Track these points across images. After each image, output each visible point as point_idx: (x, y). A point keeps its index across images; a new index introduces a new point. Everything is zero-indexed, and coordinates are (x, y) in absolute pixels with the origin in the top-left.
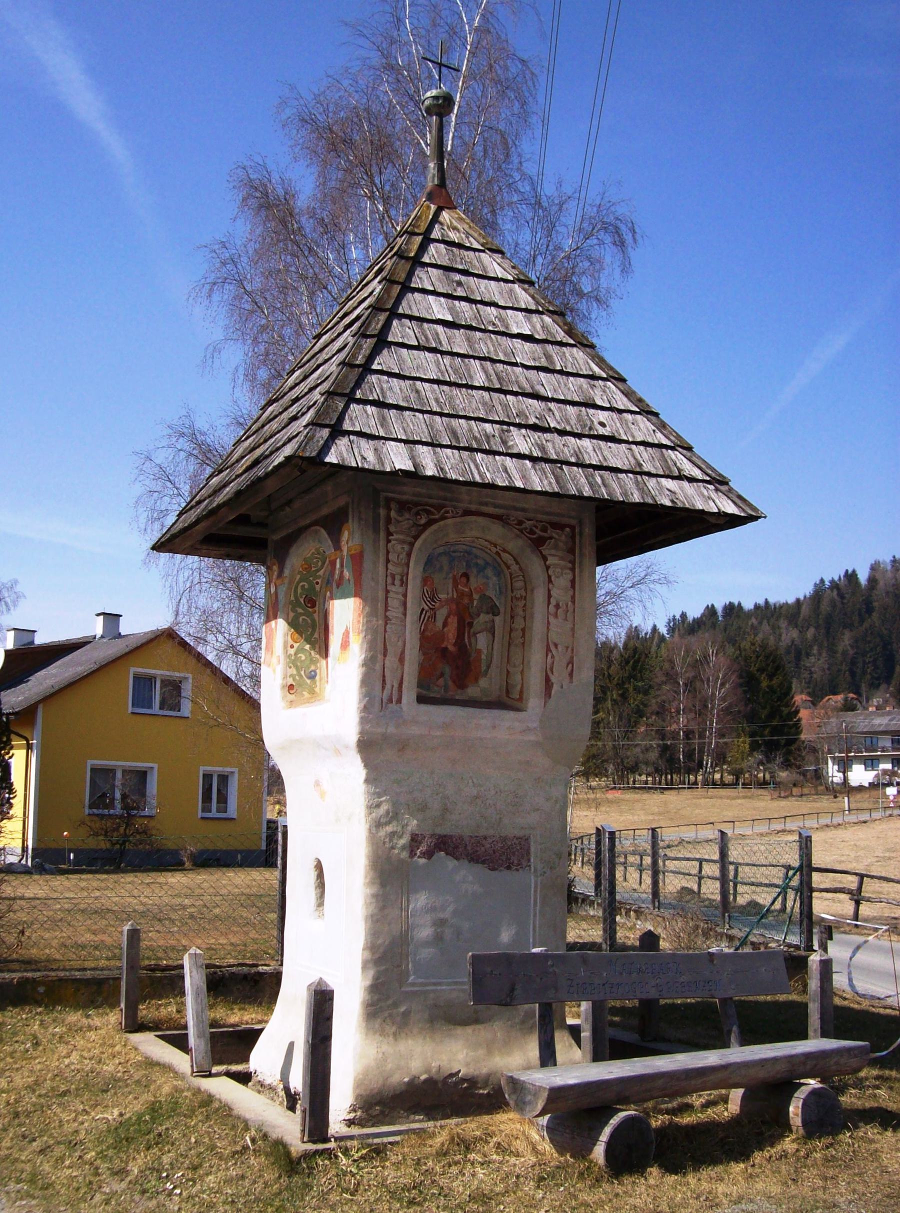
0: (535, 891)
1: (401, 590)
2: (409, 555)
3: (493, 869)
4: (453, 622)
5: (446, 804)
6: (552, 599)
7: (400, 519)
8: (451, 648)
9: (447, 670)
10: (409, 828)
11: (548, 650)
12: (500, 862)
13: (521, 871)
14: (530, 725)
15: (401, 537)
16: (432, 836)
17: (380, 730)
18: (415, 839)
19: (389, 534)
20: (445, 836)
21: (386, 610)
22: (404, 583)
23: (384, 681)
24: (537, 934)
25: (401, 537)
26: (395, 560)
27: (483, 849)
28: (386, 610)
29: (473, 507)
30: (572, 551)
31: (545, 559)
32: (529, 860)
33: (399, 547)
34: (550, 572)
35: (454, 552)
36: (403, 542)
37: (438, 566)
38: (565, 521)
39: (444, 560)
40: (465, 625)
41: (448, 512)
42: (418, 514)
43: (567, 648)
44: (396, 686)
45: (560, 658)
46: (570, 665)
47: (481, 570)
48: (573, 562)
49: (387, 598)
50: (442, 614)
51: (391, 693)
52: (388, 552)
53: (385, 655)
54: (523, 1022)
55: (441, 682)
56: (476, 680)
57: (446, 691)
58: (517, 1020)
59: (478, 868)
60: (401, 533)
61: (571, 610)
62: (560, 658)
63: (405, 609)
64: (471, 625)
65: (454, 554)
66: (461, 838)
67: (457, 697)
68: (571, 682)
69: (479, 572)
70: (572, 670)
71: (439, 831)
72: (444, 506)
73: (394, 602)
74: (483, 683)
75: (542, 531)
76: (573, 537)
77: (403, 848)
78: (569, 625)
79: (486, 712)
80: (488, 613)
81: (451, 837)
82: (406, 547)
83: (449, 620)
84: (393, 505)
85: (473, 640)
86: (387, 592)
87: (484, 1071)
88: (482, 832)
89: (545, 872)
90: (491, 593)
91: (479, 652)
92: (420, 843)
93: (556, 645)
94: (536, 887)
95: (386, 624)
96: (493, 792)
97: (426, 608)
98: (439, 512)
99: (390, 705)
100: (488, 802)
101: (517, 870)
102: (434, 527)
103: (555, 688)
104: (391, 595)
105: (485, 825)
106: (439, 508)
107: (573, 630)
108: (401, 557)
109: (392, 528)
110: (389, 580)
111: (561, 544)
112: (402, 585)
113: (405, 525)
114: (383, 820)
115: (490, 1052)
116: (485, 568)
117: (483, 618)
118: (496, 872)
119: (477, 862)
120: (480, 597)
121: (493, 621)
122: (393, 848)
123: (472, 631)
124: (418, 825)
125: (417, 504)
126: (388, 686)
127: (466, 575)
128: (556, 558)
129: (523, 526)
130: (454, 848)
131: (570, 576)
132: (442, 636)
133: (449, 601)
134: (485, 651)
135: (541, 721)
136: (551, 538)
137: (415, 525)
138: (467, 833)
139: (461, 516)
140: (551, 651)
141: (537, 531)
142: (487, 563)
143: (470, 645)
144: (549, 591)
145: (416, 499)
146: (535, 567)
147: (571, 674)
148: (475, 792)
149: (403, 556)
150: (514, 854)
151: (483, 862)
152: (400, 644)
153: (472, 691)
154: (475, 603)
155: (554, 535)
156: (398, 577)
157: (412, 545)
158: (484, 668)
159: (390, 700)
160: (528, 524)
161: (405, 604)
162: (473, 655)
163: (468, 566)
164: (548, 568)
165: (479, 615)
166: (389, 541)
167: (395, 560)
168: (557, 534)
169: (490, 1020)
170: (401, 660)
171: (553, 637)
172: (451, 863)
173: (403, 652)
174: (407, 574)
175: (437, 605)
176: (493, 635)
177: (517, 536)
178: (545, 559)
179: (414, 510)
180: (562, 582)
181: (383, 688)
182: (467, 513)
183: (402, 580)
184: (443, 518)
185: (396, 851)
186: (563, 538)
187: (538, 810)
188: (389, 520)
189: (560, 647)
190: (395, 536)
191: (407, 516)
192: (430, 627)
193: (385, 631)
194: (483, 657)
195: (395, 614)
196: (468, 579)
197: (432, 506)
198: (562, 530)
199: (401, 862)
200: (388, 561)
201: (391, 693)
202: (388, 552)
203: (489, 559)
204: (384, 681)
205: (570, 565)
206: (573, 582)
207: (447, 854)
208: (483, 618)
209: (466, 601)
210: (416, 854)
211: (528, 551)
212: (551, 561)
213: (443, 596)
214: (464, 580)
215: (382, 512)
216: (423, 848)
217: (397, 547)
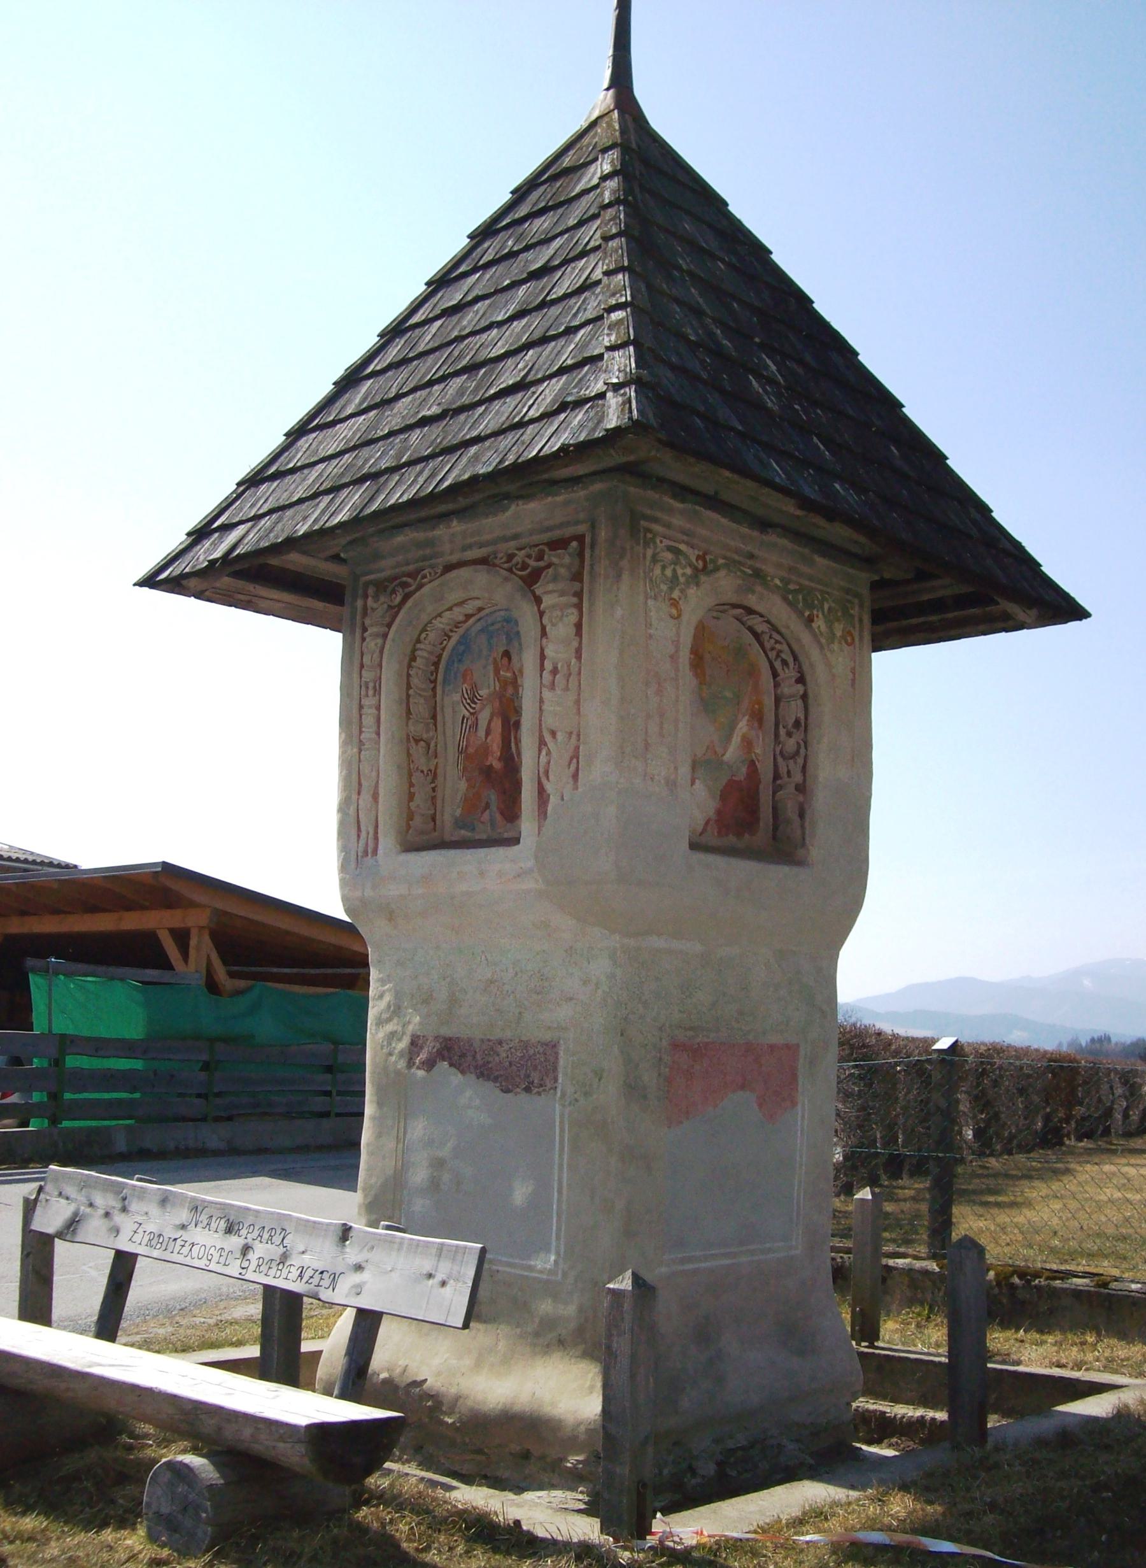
0: (562, 1130)
3: (507, 1091)
4: (497, 724)
6: (546, 662)
8: (497, 765)
10: (411, 1027)
12: (518, 1080)
16: (436, 1038)
17: (358, 894)
18: (416, 1043)
19: (365, 630)
20: (450, 1039)
21: (361, 732)
22: (377, 691)
24: (564, 1198)
27: (497, 1058)
29: (454, 558)
30: (577, 577)
31: (538, 600)
32: (556, 1080)
36: (377, 635)
38: (569, 531)
41: (424, 577)
43: (571, 733)
44: (371, 835)
46: (575, 761)
48: (579, 595)
50: (484, 717)
53: (359, 794)
54: (537, 1334)
58: (529, 1329)
59: (489, 1089)
61: (574, 670)
62: (559, 749)
63: (379, 727)
65: (491, 628)
66: (470, 1041)
68: (576, 788)
70: (577, 769)
71: (446, 1031)
76: (581, 555)
77: (401, 1054)
78: (572, 696)
82: (380, 641)
83: (493, 724)
86: (361, 707)
87: (453, 1390)
88: (497, 1034)
89: (576, 1100)
92: (422, 1048)
94: (562, 1122)
95: (360, 751)
98: (415, 579)
100: (507, 987)
101: (539, 1093)
103: (553, 800)
104: (364, 711)
109: (367, 622)
111: (562, 571)
112: (374, 695)
113: (380, 612)
114: (385, 1016)
115: (478, 1365)
118: (510, 1095)
119: (488, 1079)
122: (390, 1054)
124: (420, 1023)
126: (363, 834)
128: (556, 595)
129: (514, 561)
131: (573, 618)
132: (485, 750)
135: (536, 857)
136: (549, 566)
140: (546, 744)
144: (542, 650)
146: (526, 614)
147: (575, 776)
150: (535, 1068)
151: (496, 1079)
152: (374, 774)
155: (555, 560)
156: (371, 685)
157: (385, 636)
159: (366, 853)
164: (541, 614)
169: (495, 1321)
170: (375, 797)
171: (549, 721)
172: (456, 1078)
175: (478, 707)
177: (506, 579)
180: (561, 629)
181: (359, 836)
182: (449, 568)
183: (375, 687)
184: (420, 586)
185: (393, 1058)
186: (567, 560)
187: (571, 999)
196: (510, 659)
197: (409, 575)
199: (398, 1073)
200: (362, 666)
201: (367, 844)
205: (575, 600)
206: (579, 626)
207: (451, 1065)
210: (414, 1064)
212: (547, 601)
216: (423, 1056)
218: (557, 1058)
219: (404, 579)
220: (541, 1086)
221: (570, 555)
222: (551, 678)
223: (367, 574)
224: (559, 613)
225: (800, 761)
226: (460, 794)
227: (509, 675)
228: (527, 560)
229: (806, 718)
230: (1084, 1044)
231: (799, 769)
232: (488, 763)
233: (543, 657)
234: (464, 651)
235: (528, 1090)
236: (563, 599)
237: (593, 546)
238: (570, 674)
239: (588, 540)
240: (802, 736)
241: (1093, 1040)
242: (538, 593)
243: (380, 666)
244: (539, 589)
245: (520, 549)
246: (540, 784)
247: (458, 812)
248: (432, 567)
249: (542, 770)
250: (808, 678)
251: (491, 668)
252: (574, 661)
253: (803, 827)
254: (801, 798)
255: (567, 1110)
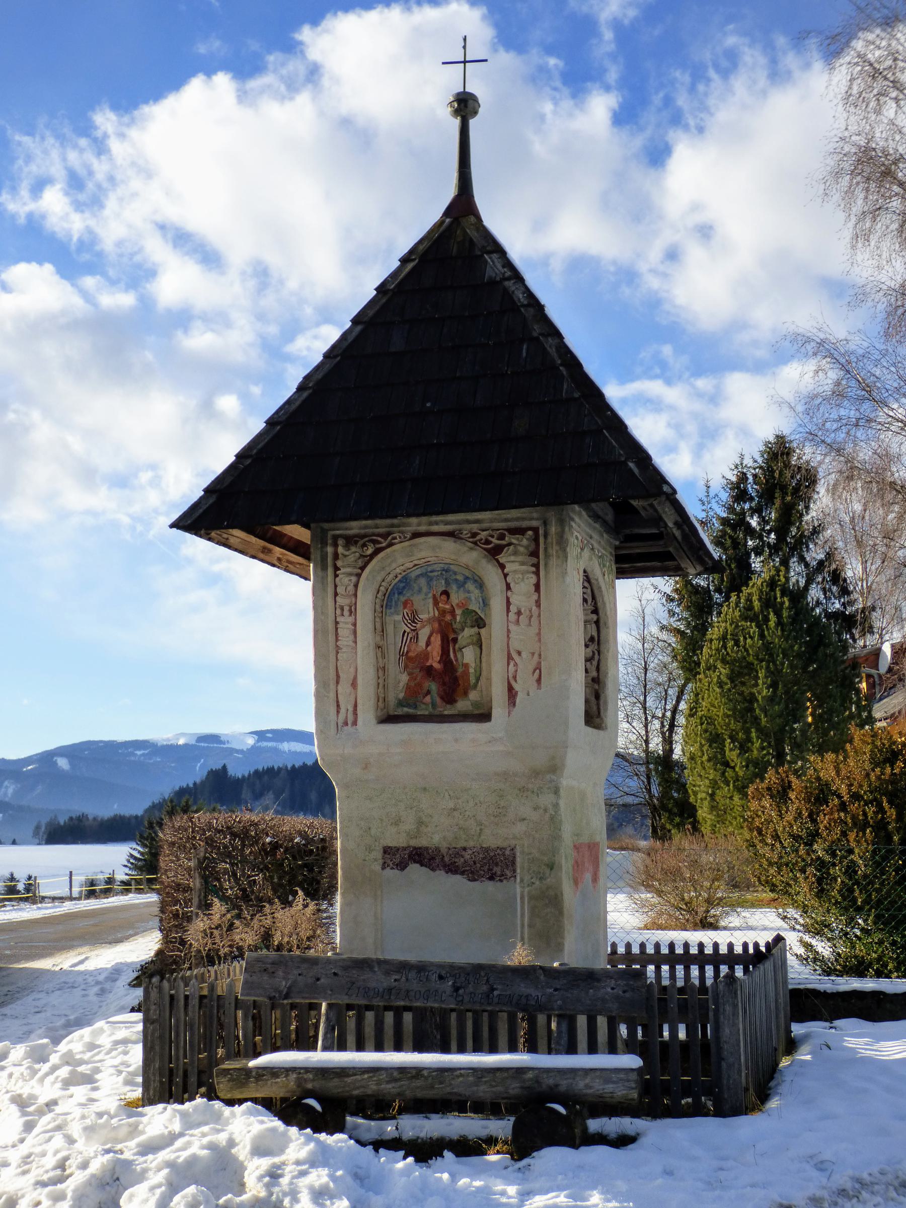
1: (351, 619)
2: (356, 586)
4: (437, 641)
5: (420, 818)
7: (347, 553)
8: (437, 666)
9: (434, 687)
11: (510, 658)
12: (482, 873)
13: (505, 882)
14: (494, 736)
15: (349, 570)
19: (336, 569)
20: (420, 848)
21: (337, 640)
22: (353, 611)
23: (338, 706)
25: (349, 570)
26: (343, 593)
27: (462, 860)
28: (337, 640)
30: (535, 554)
31: (502, 567)
32: (514, 871)
33: (346, 580)
34: (509, 579)
35: (431, 572)
37: (416, 588)
38: (525, 524)
39: (423, 581)
40: (448, 640)
41: (395, 538)
42: (364, 545)
43: (533, 654)
44: (351, 709)
45: (525, 665)
47: (461, 585)
48: (537, 566)
49: (337, 629)
50: (424, 634)
51: (347, 717)
52: (336, 586)
55: (428, 699)
56: (466, 694)
57: (434, 705)
60: (349, 566)
62: (525, 665)
63: (355, 637)
64: (455, 640)
66: (438, 849)
67: (446, 713)
69: (459, 588)
71: (414, 843)
72: (389, 534)
73: (345, 631)
74: (473, 695)
75: (498, 539)
76: (536, 540)
78: (534, 630)
79: (445, 726)
80: (472, 627)
81: (427, 848)
82: (354, 579)
83: (432, 638)
84: (341, 542)
85: (459, 655)
86: (337, 623)
88: (461, 844)
90: (473, 606)
91: (466, 666)
93: (519, 653)
94: (522, 898)
96: (471, 804)
97: (408, 630)
99: (346, 728)
101: (501, 881)
102: (381, 555)
105: (464, 836)
106: (385, 536)
107: (539, 634)
108: (349, 588)
109: (339, 563)
110: (338, 612)
111: (521, 549)
112: (350, 615)
113: (352, 558)
116: (465, 583)
117: (468, 632)
120: (463, 611)
121: (479, 634)
123: (457, 646)
125: (363, 536)
126: (343, 710)
127: (446, 593)
129: (478, 538)
130: (430, 860)
131: (533, 580)
132: (426, 655)
133: (429, 621)
134: (473, 665)
136: (510, 544)
137: (362, 556)
138: (444, 846)
139: (411, 539)
140: (513, 659)
141: (494, 540)
142: (467, 578)
143: (457, 660)
145: (363, 531)
147: (539, 681)
148: (451, 805)
149: (351, 588)
150: (497, 865)
151: (462, 873)
152: (352, 670)
153: (462, 705)
154: (458, 618)
155: (514, 541)
157: (359, 576)
158: (472, 680)
160: (483, 535)
161: (355, 633)
162: (460, 670)
163: (447, 583)
164: (506, 576)
165: (463, 630)
166: (336, 576)
167: (343, 593)
168: (518, 539)
170: (354, 684)
171: (515, 645)
173: (355, 678)
174: (356, 604)
175: (418, 626)
176: (481, 647)
177: (471, 549)
178: (502, 567)
179: (361, 542)
180: (522, 587)
181: (338, 712)
183: (350, 612)
184: (390, 545)
186: (525, 542)
187: (524, 819)
188: (336, 556)
189: (524, 655)
190: (343, 570)
191: (353, 549)
192: (413, 647)
193: (337, 660)
194: (471, 670)
195: (345, 643)
198: (523, 535)
200: (336, 594)
201: (347, 717)
202: (336, 586)
203: (467, 574)
204: (338, 706)
205: (534, 569)
206: (537, 587)
208: (468, 632)
209: (448, 618)
211: (484, 562)
213: (424, 616)
214: (444, 597)
215: (330, 550)
217: (345, 581)
218: (514, 857)
219: (374, 538)
220: (503, 875)
221: (527, 539)
222: (516, 617)
223: (334, 530)
224: (521, 576)
225: (595, 663)
226: (401, 685)
227: (447, 607)
228: (490, 538)
229: (599, 636)
230: (62, 823)
231: (594, 668)
232: (428, 664)
233: (508, 603)
234: (404, 588)
235: (491, 878)
236: (524, 568)
237: (546, 536)
238: (531, 616)
239: (541, 532)
240: (596, 647)
241: (71, 819)
242: (501, 561)
243: (355, 595)
244: (502, 558)
245: (483, 530)
246: (509, 683)
247: (401, 695)
248: (402, 532)
249: (511, 676)
250: (600, 612)
251: (431, 601)
252: (534, 608)
253: (598, 705)
254: (596, 687)
255: (526, 890)
